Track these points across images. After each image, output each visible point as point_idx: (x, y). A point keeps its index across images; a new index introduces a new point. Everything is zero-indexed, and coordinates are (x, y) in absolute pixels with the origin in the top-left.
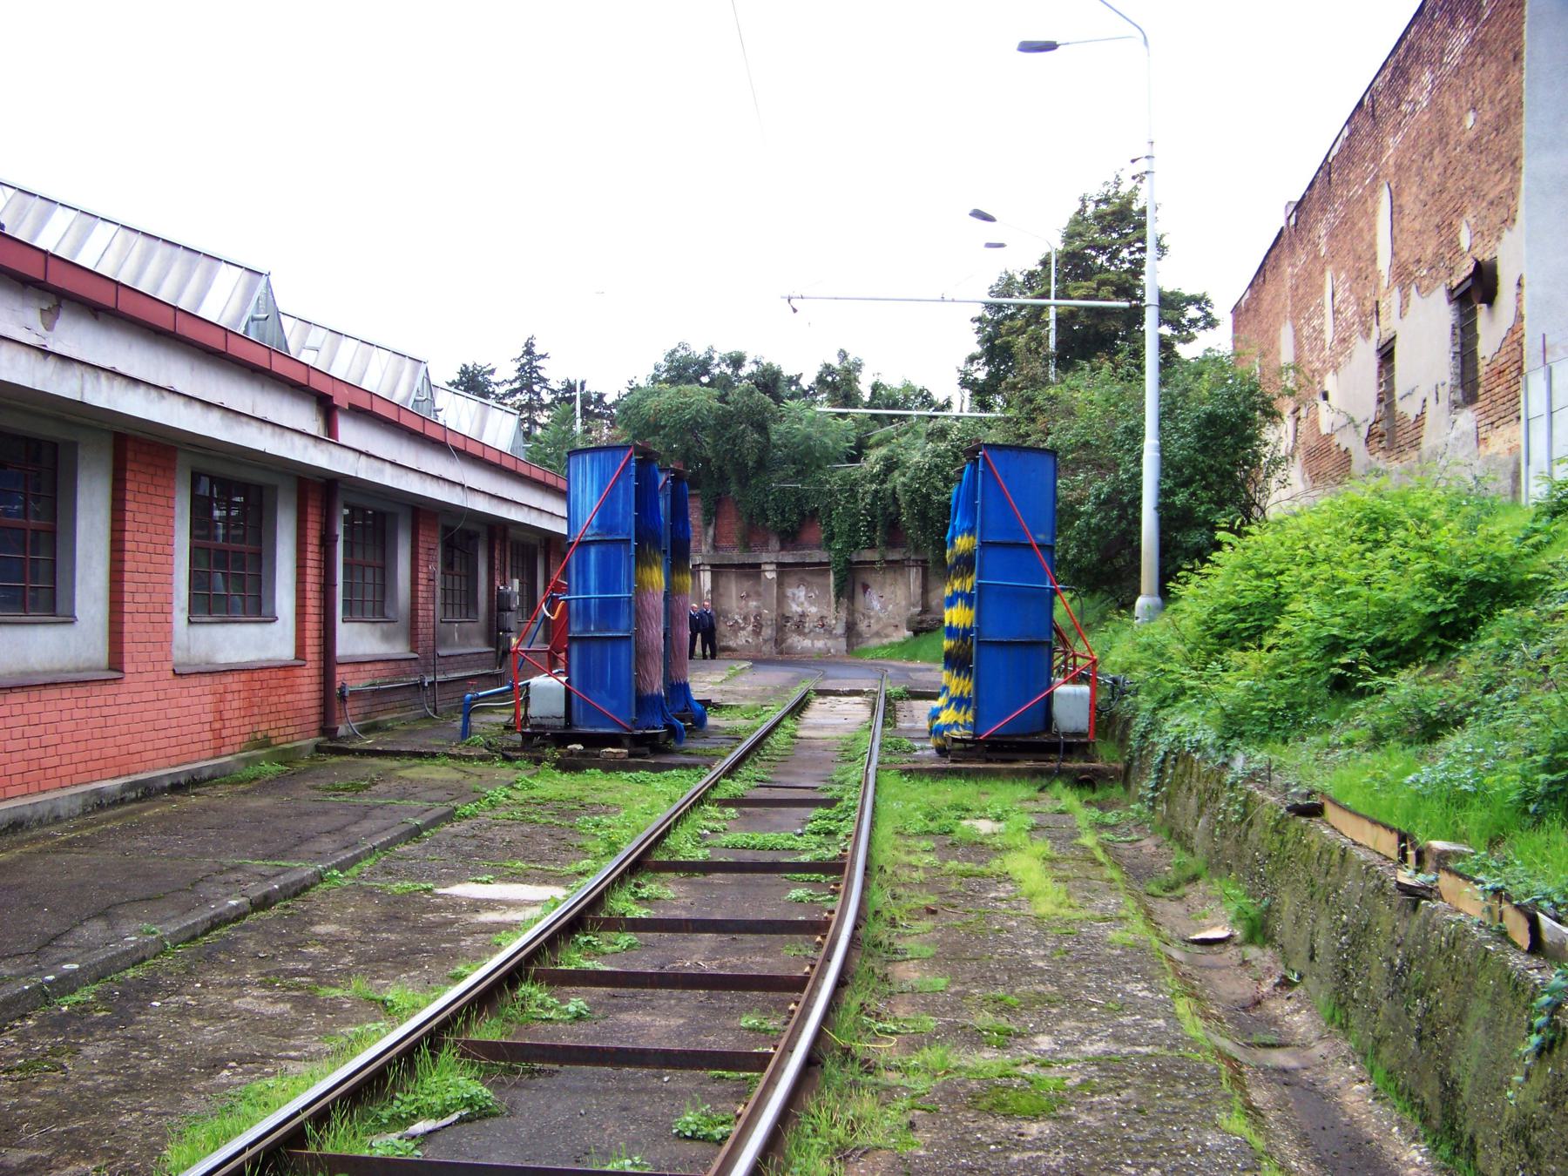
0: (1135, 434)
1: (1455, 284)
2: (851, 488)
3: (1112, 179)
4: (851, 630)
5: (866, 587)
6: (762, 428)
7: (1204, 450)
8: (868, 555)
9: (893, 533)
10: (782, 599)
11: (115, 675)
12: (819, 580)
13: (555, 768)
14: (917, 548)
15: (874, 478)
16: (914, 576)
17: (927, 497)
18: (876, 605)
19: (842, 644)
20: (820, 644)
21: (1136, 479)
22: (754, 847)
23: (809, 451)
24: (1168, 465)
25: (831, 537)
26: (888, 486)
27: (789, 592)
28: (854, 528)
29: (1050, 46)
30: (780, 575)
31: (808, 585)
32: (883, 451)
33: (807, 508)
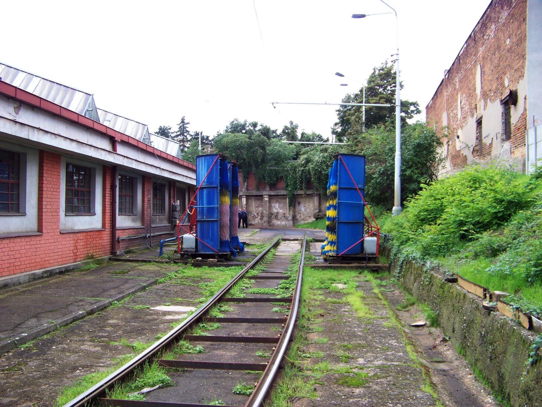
0: (392, 150)
1: (503, 98)
2: (294, 169)
3: (384, 62)
4: (294, 218)
5: (299, 203)
6: (263, 148)
7: (416, 156)
8: (300, 192)
9: (309, 184)
10: (270, 207)
11: (40, 234)
12: (283, 201)
13: (192, 266)
14: (317, 190)
15: (302, 165)
16: (316, 199)
17: (320, 172)
18: (303, 209)
19: (291, 223)
20: (283, 223)
21: (393, 166)
22: (261, 293)
23: (280, 156)
24: (404, 161)
25: (287, 186)
26: (307, 168)
27: (273, 205)
28: (295, 183)
29: (363, 16)
30: (270, 199)
31: (279, 203)
32: (305, 156)
33: (279, 176)
